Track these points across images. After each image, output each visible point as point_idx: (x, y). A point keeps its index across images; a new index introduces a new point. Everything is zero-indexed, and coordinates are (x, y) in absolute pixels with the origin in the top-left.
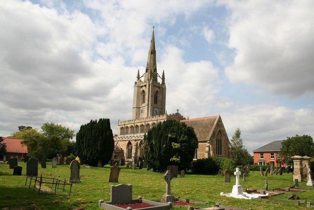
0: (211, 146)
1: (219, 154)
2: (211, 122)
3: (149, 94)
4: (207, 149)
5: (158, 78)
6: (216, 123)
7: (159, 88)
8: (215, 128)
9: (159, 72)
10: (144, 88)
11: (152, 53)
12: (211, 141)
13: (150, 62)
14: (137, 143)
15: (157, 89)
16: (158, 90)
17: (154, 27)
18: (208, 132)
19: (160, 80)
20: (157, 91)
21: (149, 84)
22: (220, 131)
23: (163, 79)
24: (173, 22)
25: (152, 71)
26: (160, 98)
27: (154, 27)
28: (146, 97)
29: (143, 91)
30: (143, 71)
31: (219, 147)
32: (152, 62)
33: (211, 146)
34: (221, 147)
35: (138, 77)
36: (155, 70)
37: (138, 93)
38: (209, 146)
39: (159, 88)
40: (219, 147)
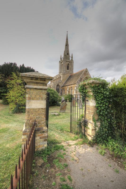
9: (70, 55)
15: (68, 63)
17: (67, 32)
19: (71, 59)
20: (68, 64)
23: (72, 57)
25: (67, 53)
26: (70, 67)
27: (67, 32)
29: (62, 64)
30: (63, 56)
35: (61, 59)
36: (68, 54)
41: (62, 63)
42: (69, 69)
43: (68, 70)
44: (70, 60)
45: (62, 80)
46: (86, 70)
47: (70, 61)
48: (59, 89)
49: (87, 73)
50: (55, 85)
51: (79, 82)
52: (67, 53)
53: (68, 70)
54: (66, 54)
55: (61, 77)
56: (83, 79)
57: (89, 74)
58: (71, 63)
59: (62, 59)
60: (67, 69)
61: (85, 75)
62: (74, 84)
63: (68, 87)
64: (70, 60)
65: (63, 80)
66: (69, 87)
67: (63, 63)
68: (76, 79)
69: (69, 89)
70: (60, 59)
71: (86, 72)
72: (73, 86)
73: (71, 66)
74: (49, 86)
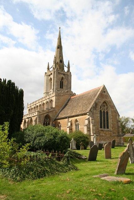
0: (91, 119)
1: (104, 128)
2: (95, 91)
3: (54, 80)
4: (87, 122)
5: (65, 67)
6: (99, 93)
7: (64, 75)
8: (97, 99)
9: (66, 63)
10: (51, 76)
11: (58, 48)
12: (91, 112)
13: (57, 55)
14: (29, 120)
15: (62, 76)
16: (64, 76)
17: (60, 28)
18: (90, 104)
19: (66, 69)
20: (62, 78)
21: (54, 72)
22: (105, 102)
23: (69, 67)
24: (109, 51)
25: (59, 62)
26: (65, 83)
27: (60, 28)
28: (52, 81)
29: (51, 79)
30: (52, 64)
31: (104, 121)
32: (58, 55)
33: (91, 119)
34: (108, 121)
35: (48, 69)
36: (61, 61)
37: (47, 80)
38: (88, 119)
39: (64, 75)
40: (104, 121)
41: (50, 75)
42: (63, 87)
43: (62, 88)
44: (66, 71)
45: (54, 106)
46: (103, 87)
47: (64, 73)
48: (107, 113)
49: (105, 94)
50: (42, 115)
51: (92, 110)
52: (59, 62)
53: (62, 88)
54: (58, 61)
55: (52, 100)
56: (100, 104)
57: (109, 96)
58: (68, 77)
59: (51, 70)
60: (61, 88)
61: (103, 98)
62: (82, 115)
63: (68, 120)
64: (66, 71)
65: (56, 106)
66: (70, 119)
67: (52, 76)
68: (86, 105)
69: (71, 124)
70: (47, 70)
71: (104, 92)
72: (80, 119)
73: (66, 82)
74: (28, 118)
